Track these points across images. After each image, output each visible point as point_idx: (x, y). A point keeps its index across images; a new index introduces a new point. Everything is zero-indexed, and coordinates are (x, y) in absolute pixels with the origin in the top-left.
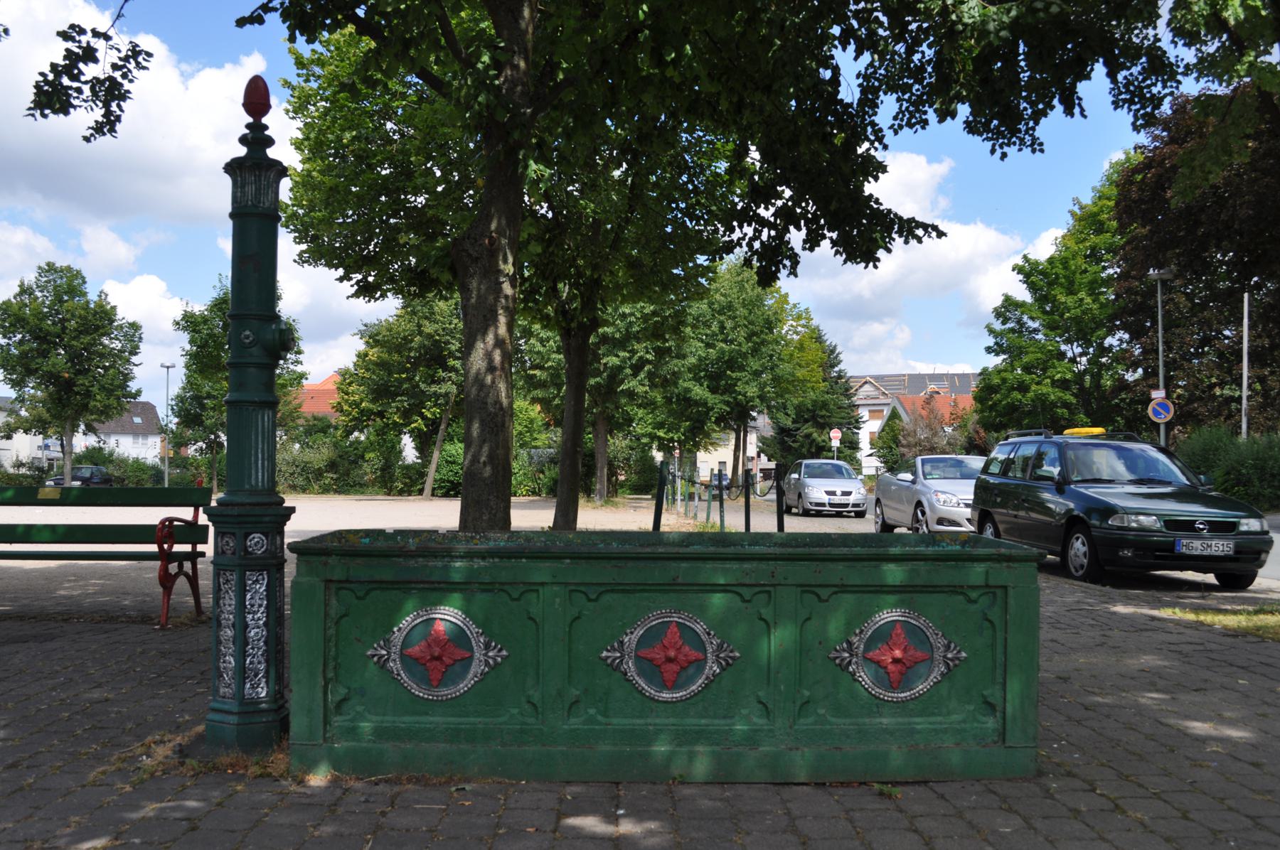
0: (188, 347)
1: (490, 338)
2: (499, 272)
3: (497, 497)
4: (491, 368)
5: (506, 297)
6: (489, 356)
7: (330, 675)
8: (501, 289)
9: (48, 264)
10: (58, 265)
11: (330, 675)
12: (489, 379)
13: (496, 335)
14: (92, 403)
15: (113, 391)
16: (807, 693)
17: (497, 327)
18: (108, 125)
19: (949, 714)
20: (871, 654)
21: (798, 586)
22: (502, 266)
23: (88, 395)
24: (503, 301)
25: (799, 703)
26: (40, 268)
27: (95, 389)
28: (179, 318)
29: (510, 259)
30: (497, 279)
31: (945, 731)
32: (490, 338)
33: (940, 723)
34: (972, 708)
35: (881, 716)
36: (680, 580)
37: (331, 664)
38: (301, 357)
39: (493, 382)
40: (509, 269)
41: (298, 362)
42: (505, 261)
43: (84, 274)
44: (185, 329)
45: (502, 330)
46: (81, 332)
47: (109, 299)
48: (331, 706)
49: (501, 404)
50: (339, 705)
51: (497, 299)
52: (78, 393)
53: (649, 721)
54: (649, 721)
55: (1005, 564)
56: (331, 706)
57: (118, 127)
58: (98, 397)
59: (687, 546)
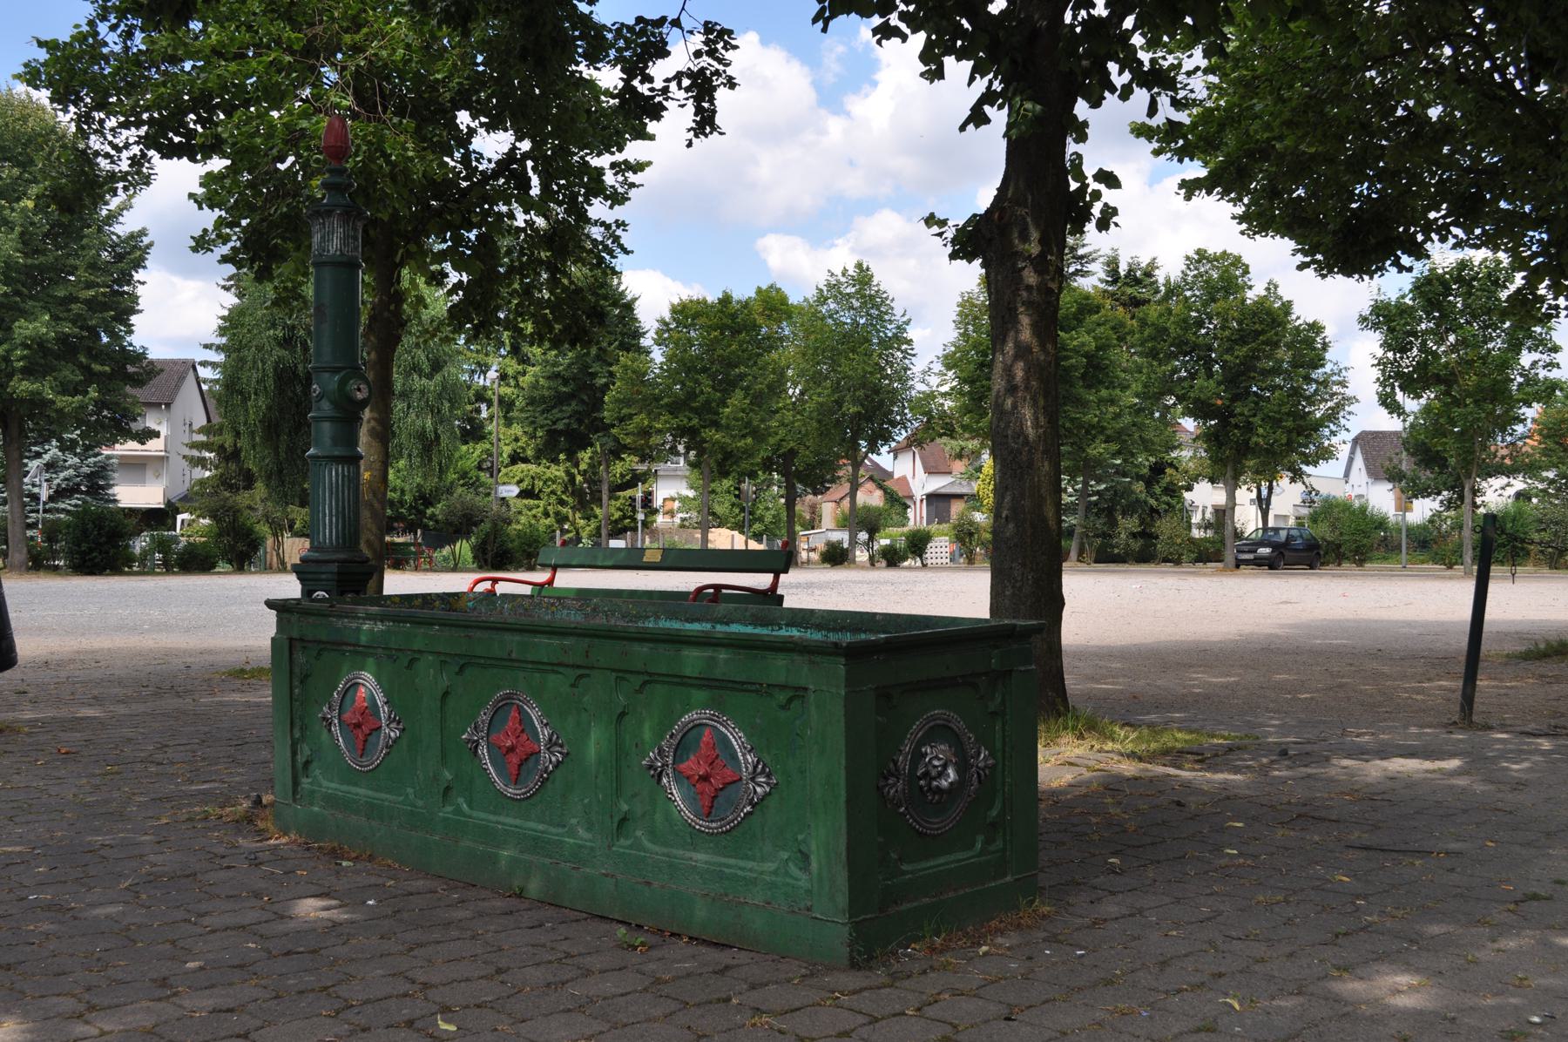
0: (1380, 353)
1: (1010, 347)
2: (1017, 255)
3: (1024, 565)
4: (1012, 389)
5: (1029, 288)
6: (1008, 371)
7: (297, 735)
8: (1021, 278)
9: (1198, 252)
10: (1210, 251)
11: (297, 735)
12: (1009, 402)
13: (1018, 344)
14: (1255, 439)
15: (1280, 420)
16: (625, 807)
17: (1017, 332)
18: (705, 122)
19: (763, 859)
20: (683, 766)
21: (613, 670)
22: (1021, 247)
23: (1249, 428)
24: (1025, 294)
25: (616, 820)
26: (1188, 258)
27: (1257, 420)
28: (1366, 312)
29: (1035, 235)
30: (1014, 265)
31: (754, 882)
32: (1010, 347)
33: (751, 870)
34: (785, 855)
35: (695, 850)
36: (514, 656)
37: (298, 722)
38: (1558, 357)
39: (1015, 406)
40: (1034, 249)
41: (1551, 365)
42: (1025, 238)
43: (1245, 260)
44: (1376, 326)
45: (1026, 335)
46: (1235, 342)
47: (1280, 291)
48: (300, 765)
49: (1026, 437)
50: (307, 764)
51: (1016, 293)
52: (1236, 426)
53: (501, 819)
54: (501, 819)
55: (806, 657)
56: (300, 765)
57: (718, 120)
58: (1261, 431)
59: (727, 624)
